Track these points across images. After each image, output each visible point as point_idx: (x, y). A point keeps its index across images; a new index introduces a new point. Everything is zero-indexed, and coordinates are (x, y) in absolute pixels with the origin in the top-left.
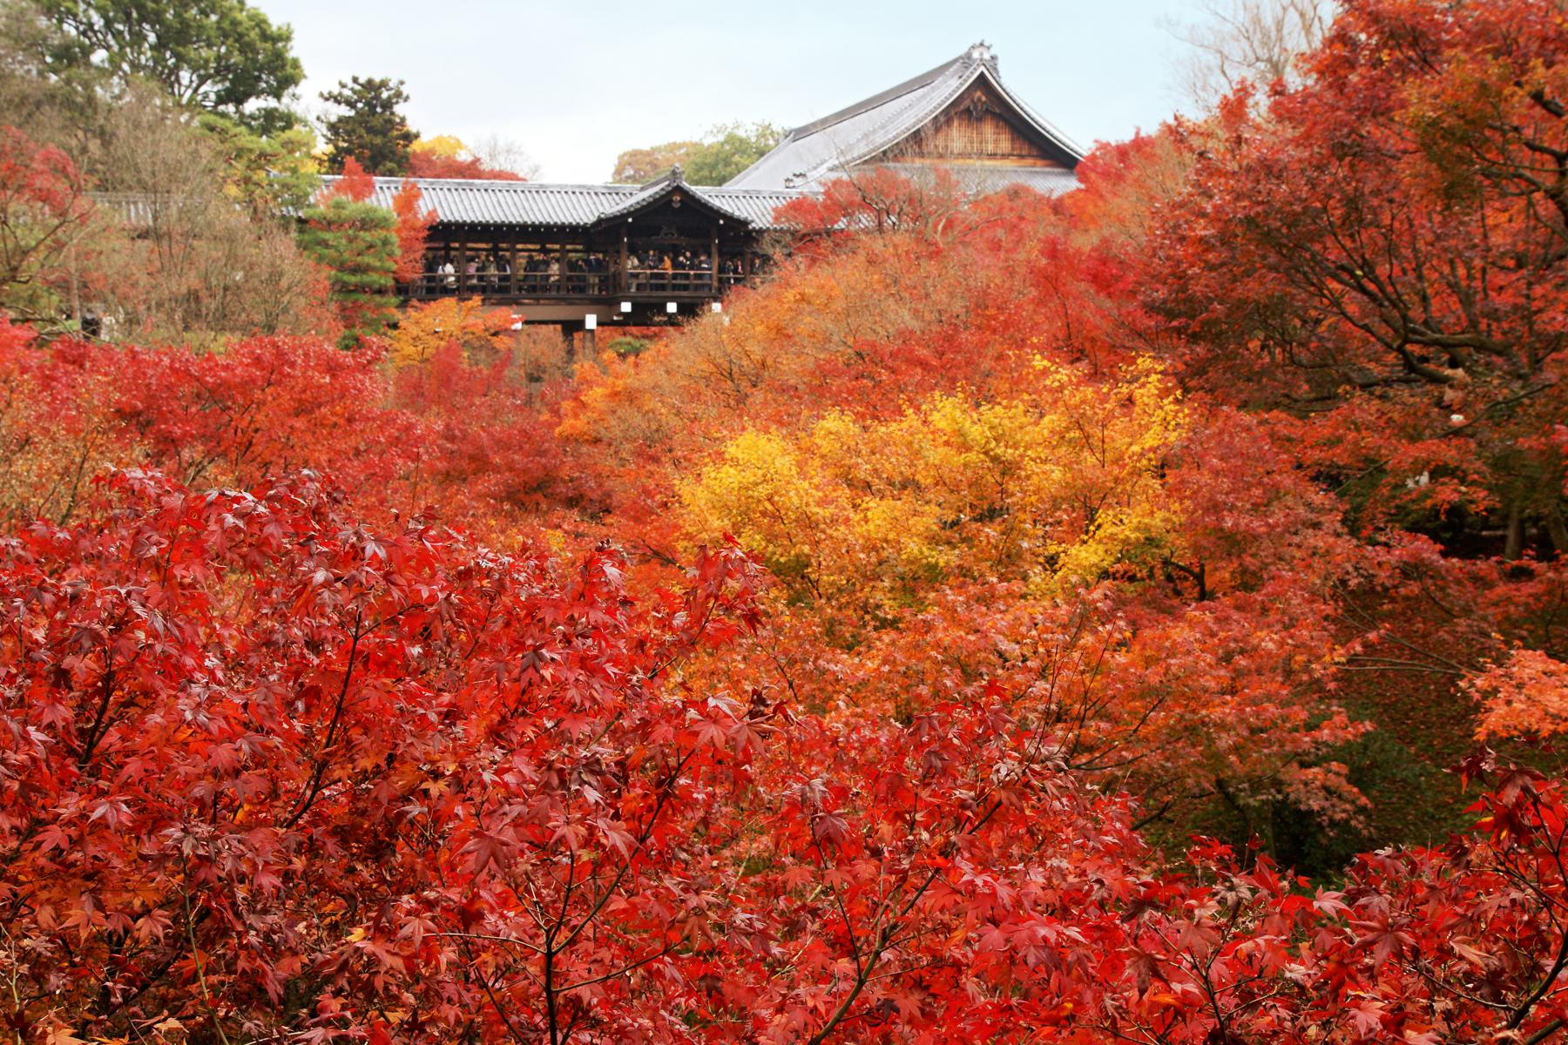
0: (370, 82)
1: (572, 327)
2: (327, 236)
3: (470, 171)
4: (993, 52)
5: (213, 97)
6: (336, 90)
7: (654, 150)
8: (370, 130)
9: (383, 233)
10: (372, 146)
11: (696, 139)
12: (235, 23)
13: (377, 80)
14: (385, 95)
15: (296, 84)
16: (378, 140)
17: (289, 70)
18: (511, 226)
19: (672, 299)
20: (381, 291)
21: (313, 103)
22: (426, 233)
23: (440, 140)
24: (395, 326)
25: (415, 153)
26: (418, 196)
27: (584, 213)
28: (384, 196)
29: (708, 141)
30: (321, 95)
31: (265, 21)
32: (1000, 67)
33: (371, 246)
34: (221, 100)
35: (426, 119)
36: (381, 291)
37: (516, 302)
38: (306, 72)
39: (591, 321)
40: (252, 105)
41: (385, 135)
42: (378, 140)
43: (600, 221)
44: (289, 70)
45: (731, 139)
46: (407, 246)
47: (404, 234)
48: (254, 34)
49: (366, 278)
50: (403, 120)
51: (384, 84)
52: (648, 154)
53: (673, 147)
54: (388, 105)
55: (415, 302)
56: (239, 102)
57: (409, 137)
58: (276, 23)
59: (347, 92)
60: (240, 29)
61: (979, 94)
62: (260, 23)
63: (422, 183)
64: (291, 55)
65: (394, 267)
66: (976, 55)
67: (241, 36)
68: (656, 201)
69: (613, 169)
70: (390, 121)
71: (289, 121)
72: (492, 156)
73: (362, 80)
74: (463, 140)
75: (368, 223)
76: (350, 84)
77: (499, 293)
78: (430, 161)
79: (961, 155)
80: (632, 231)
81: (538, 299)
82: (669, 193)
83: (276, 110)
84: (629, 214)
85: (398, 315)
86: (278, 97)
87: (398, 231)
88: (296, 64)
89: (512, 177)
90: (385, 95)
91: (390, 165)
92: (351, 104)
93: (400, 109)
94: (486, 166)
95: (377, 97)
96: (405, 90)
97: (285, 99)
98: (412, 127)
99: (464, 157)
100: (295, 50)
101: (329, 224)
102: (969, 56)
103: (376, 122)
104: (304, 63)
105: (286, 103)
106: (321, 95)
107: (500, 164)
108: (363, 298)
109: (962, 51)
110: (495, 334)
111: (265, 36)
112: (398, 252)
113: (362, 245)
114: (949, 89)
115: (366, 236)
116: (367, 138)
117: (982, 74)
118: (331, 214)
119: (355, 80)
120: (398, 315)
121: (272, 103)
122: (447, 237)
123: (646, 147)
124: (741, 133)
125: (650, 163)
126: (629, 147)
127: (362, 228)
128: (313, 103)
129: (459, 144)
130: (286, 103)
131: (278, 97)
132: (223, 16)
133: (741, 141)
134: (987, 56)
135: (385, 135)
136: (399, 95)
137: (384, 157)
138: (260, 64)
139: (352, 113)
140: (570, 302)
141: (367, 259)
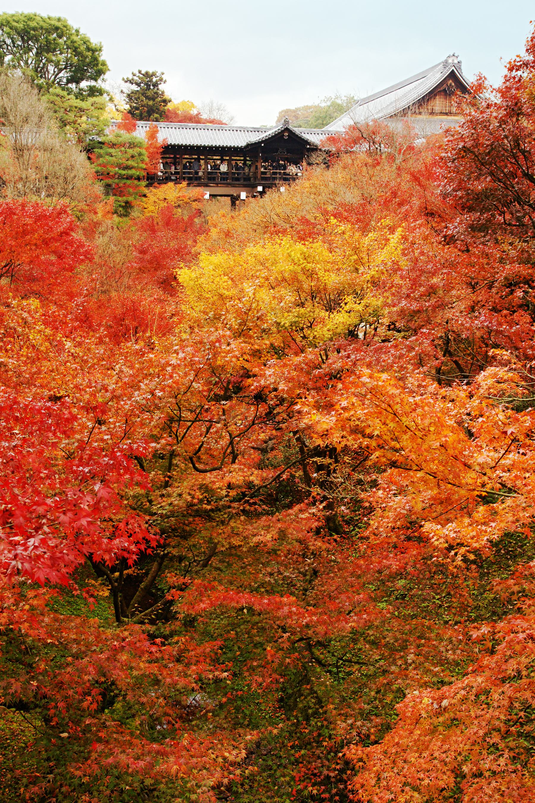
0: (147, 73)
1: (234, 199)
2: (112, 151)
3: (195, 119)
4: (459, 59)
5: (65, 80)
6: (130, 77)
7: (297, 109)
8: (147, 98)
9: (138, 149)
10: (148, 106)
11: (316, 104)
12: (73, 42)
13: (151, 72)
14: (154, 80)
15: (104, 74)
16: (151, 103)
17: (100, 67)
18: (205, 147)
19: (260, 185)
20: (139, 179)
21: (116, 86)
22: (162, 150)
23: (183, 103)
24: (145, 196)
25: (168, 110)
26: (157, 131)
27: (240, 141)
28: (141, 131)
29: (323, 105)
30: (123, 79)
31: (88, 41)
32: (462, 68)
33: (133, 157)
34: (69, 81)
35: (176, 91)
36: (139, 179)
37: (206, 185)
38: (110, 68)
39: (243, 195)
40: (84, 84)
41: (154, 100)
42: (151, 103)
43: (248, 145)
44: (100, 67)
45: (334, 104)
46: (151, 156)
47: (151, 150)
48: (83, 48)
49: (131, 172)
50: (163, 92)
51: (154, 74)
52: (294, 111)
53: (307, 108)
54: (156, 85)
55: (156, 184)
56: (78, 83)
57: (165, 102)
58: (94, 41)
59: (136, 78)
60: (76, 45)
61: (451, 81)
62: (86, 42)
63: (162, 124)
64: (101, 59)
65: (144, 166)
66: (450, 61)
67: (76, 48)
68: (276, 135)
69: (276, 119)
70: (156, 93)
71: (101, 92)
72: (211, 111)
73: (143, 72)
74: (195, 104)
75: (132, 145)
76: (138, 74)
77: (194, 180)
78: (176, 114)
79: (441, 113)
80: (264, 150)
81: (217, 184)
82: (283, 132)
83: (95, 86)
84: (262, 142)
85: (146, 191)
86: (96, 80)
87: (147, 149)
88: (104, 64)
89: (220, 123)
90: (154, 80)
91: (156, 115)
92: (138, 85)
93: (162, 87)
94: (204, 116)
95: (151, 81)
96: (164, 77)
97: (99, 81)
98: (168, 95)
99: (194, 112)
100: (103, 56)
101: (113, 145)
102: (446, 61)
103: (149, 93)
104: (108, 63)
105: (99, 84)
106: (123, 79)
107: (215, 116)
108: (129, 182)
109: (443, 59)
110: (194, 201)
111: (88, 49)
112: (147, 159)
113: (129, 156)
114: (435, 79)
115: (130, 151)
116: (145, 101)
117: (453, 71)
118: (114, 140)
119: (140, 72)
120: (146, 191)
121: (93, 83)
122: (173, 152)
123: (293, 108)
124: (339, 102)
125: (295, 116)
126: (285, 108)
127: (129, 148)
128: (116, 86)
129: (193, 106)
130: (99, 84)
131: (96, 80)
132: (68, 38)
133: (339, 105)
134: (456, 62)
135: (154, 100)
136: (161, 80)
137: (154, 112)
138: (86, 64)
139: (139, 89)
140: (233, 186)
141: (131, 163)
